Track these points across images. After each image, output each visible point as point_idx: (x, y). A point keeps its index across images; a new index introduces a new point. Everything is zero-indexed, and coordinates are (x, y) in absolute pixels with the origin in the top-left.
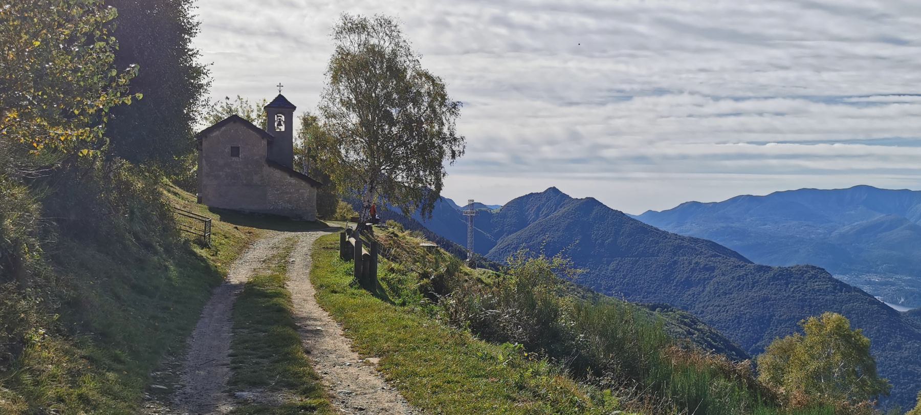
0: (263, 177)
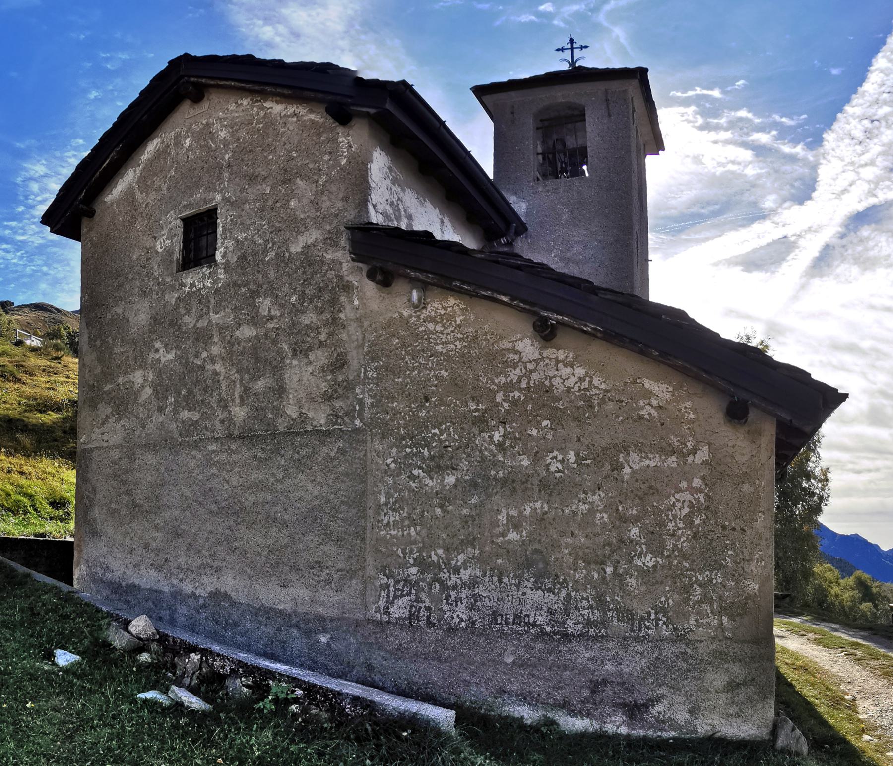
0: (339, 363)
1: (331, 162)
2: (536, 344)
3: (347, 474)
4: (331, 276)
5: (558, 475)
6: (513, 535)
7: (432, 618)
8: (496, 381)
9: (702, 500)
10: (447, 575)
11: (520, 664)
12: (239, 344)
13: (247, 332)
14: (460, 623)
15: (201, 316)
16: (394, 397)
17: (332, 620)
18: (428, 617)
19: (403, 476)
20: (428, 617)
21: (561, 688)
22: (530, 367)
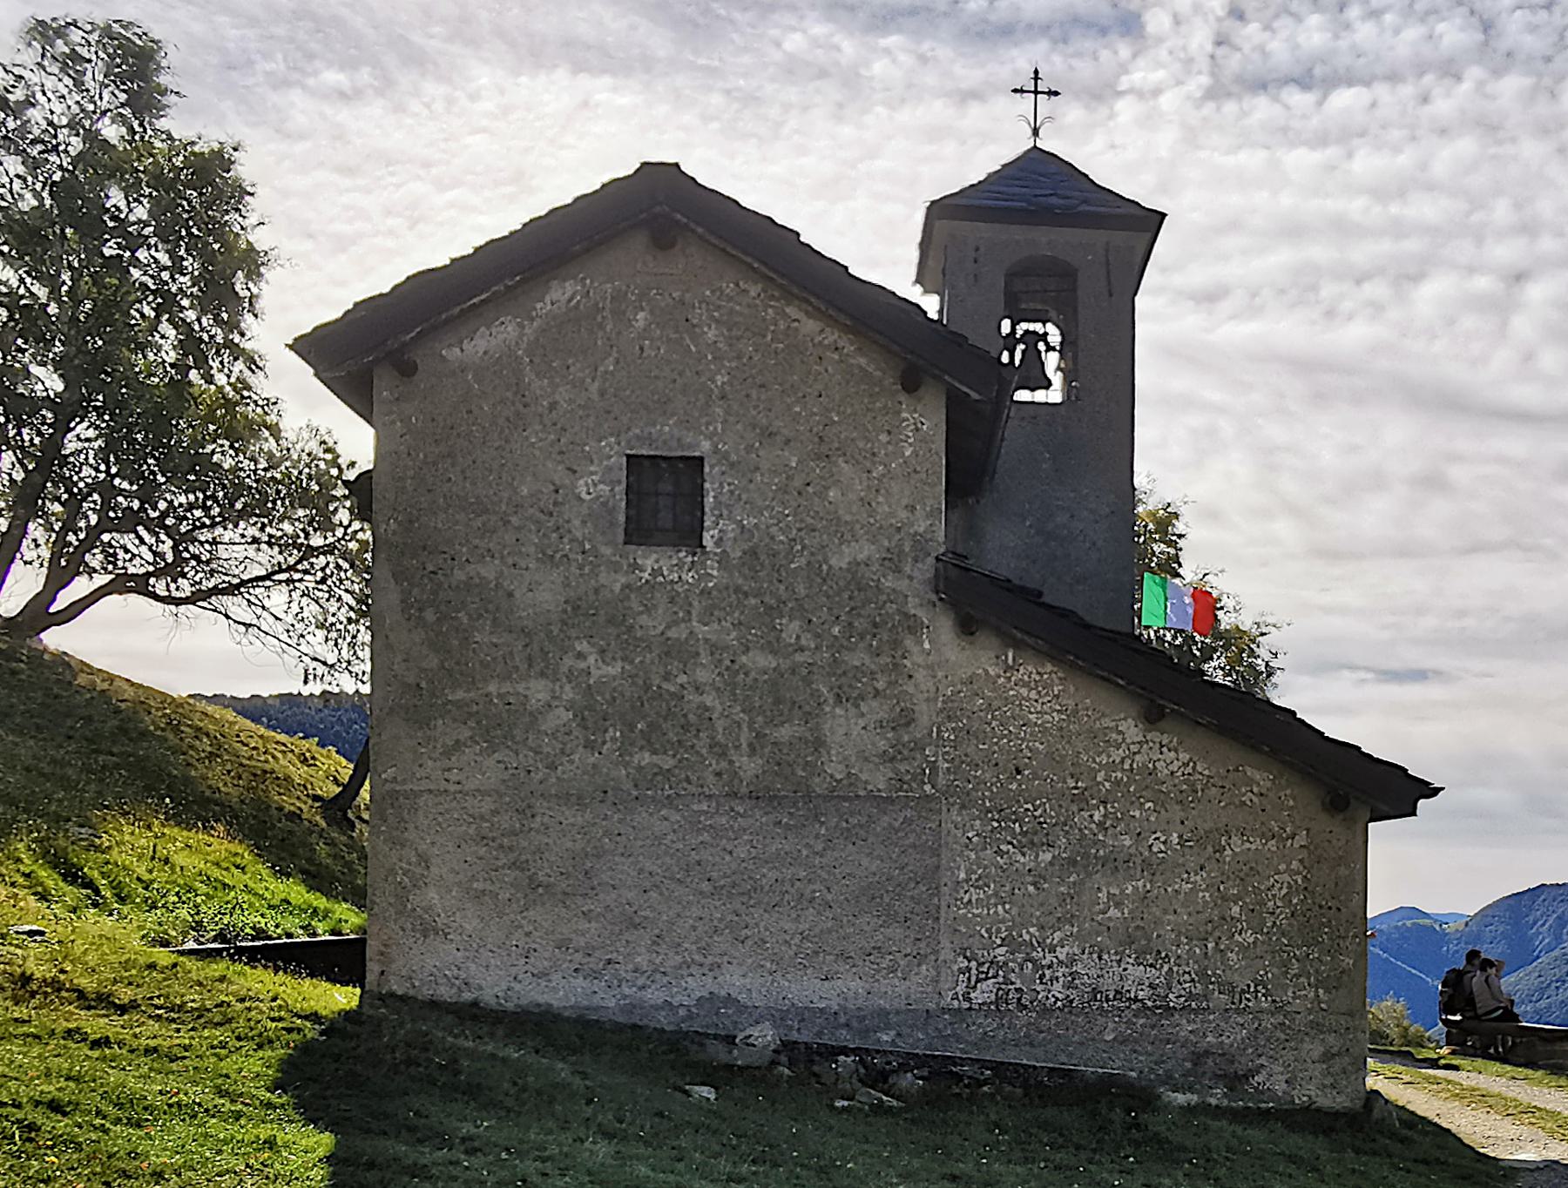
0: (906, 719)
1: (890, 448)
2: (1141, 726)
3: (914, 846)
4: (890, 611)
5: (1161, 855)
6: (1113, 912)
7: (1023, 1001)
8: (1098, 760)
9: (1300, 881)
10: (1041, 954)
11: (1121, 1040)
12: (746, 674)
13: (760, 660)
14: (1055, 1003)
15: (676, 623)
16: (977, 765)
17: (898, 1013)
18: (1019, 999)
19: (988, 852)
20: (1019, 999)
21: (1163, 1062)
22: (1134, 748)
